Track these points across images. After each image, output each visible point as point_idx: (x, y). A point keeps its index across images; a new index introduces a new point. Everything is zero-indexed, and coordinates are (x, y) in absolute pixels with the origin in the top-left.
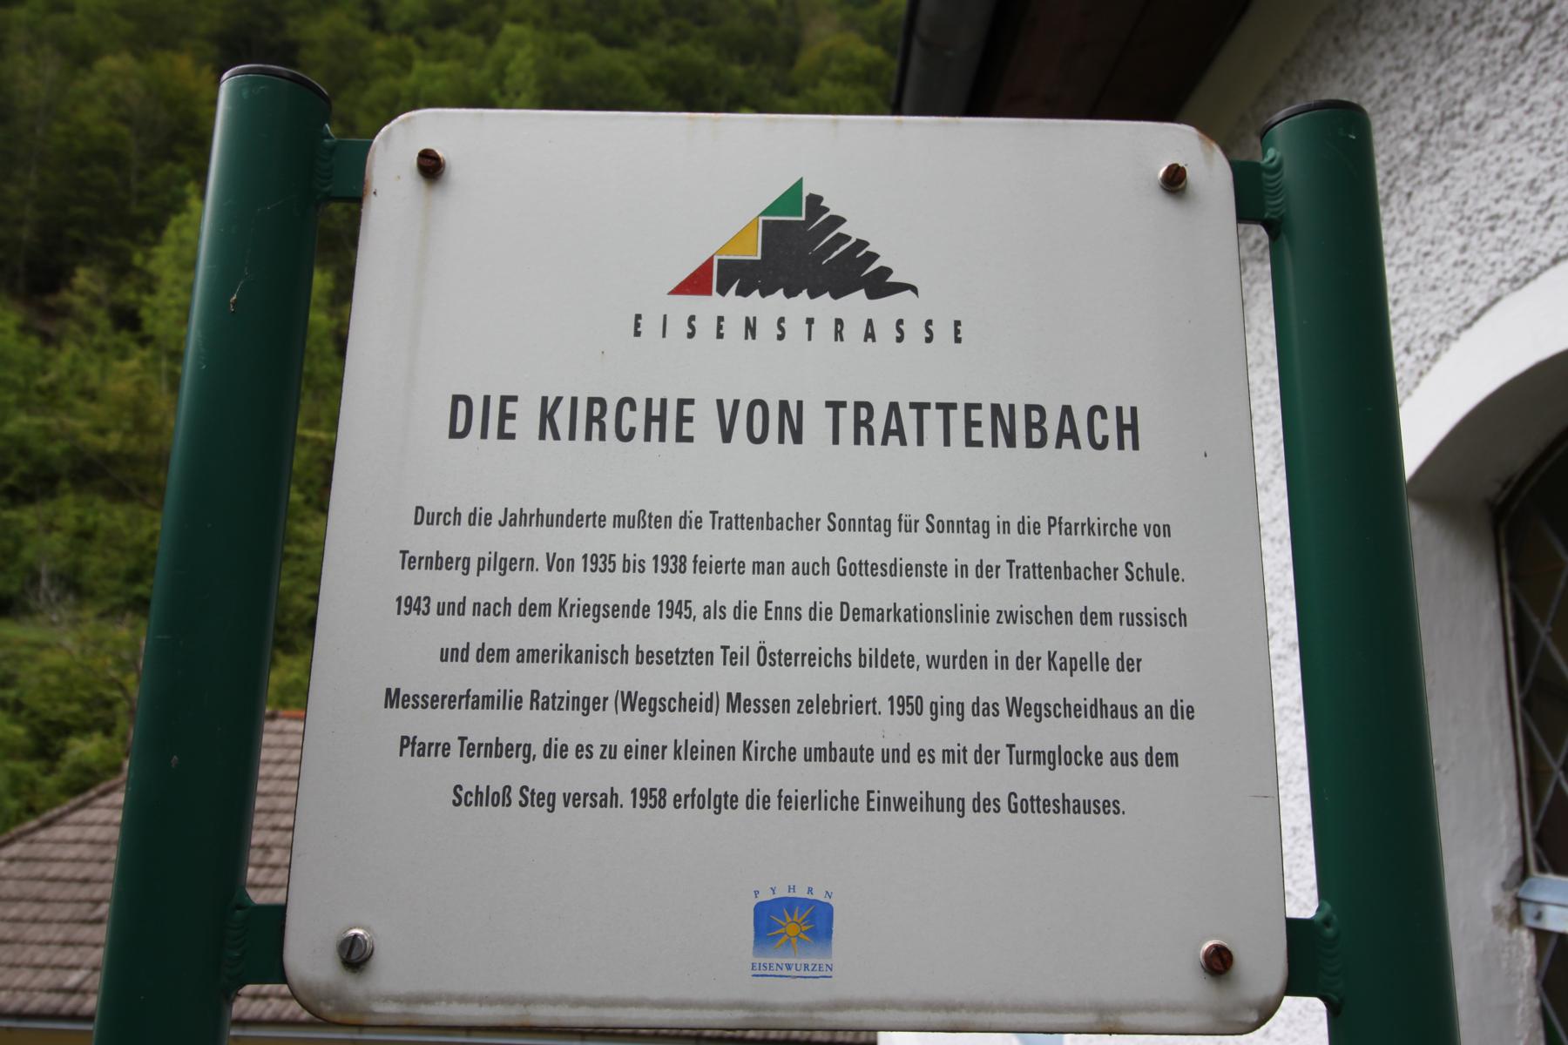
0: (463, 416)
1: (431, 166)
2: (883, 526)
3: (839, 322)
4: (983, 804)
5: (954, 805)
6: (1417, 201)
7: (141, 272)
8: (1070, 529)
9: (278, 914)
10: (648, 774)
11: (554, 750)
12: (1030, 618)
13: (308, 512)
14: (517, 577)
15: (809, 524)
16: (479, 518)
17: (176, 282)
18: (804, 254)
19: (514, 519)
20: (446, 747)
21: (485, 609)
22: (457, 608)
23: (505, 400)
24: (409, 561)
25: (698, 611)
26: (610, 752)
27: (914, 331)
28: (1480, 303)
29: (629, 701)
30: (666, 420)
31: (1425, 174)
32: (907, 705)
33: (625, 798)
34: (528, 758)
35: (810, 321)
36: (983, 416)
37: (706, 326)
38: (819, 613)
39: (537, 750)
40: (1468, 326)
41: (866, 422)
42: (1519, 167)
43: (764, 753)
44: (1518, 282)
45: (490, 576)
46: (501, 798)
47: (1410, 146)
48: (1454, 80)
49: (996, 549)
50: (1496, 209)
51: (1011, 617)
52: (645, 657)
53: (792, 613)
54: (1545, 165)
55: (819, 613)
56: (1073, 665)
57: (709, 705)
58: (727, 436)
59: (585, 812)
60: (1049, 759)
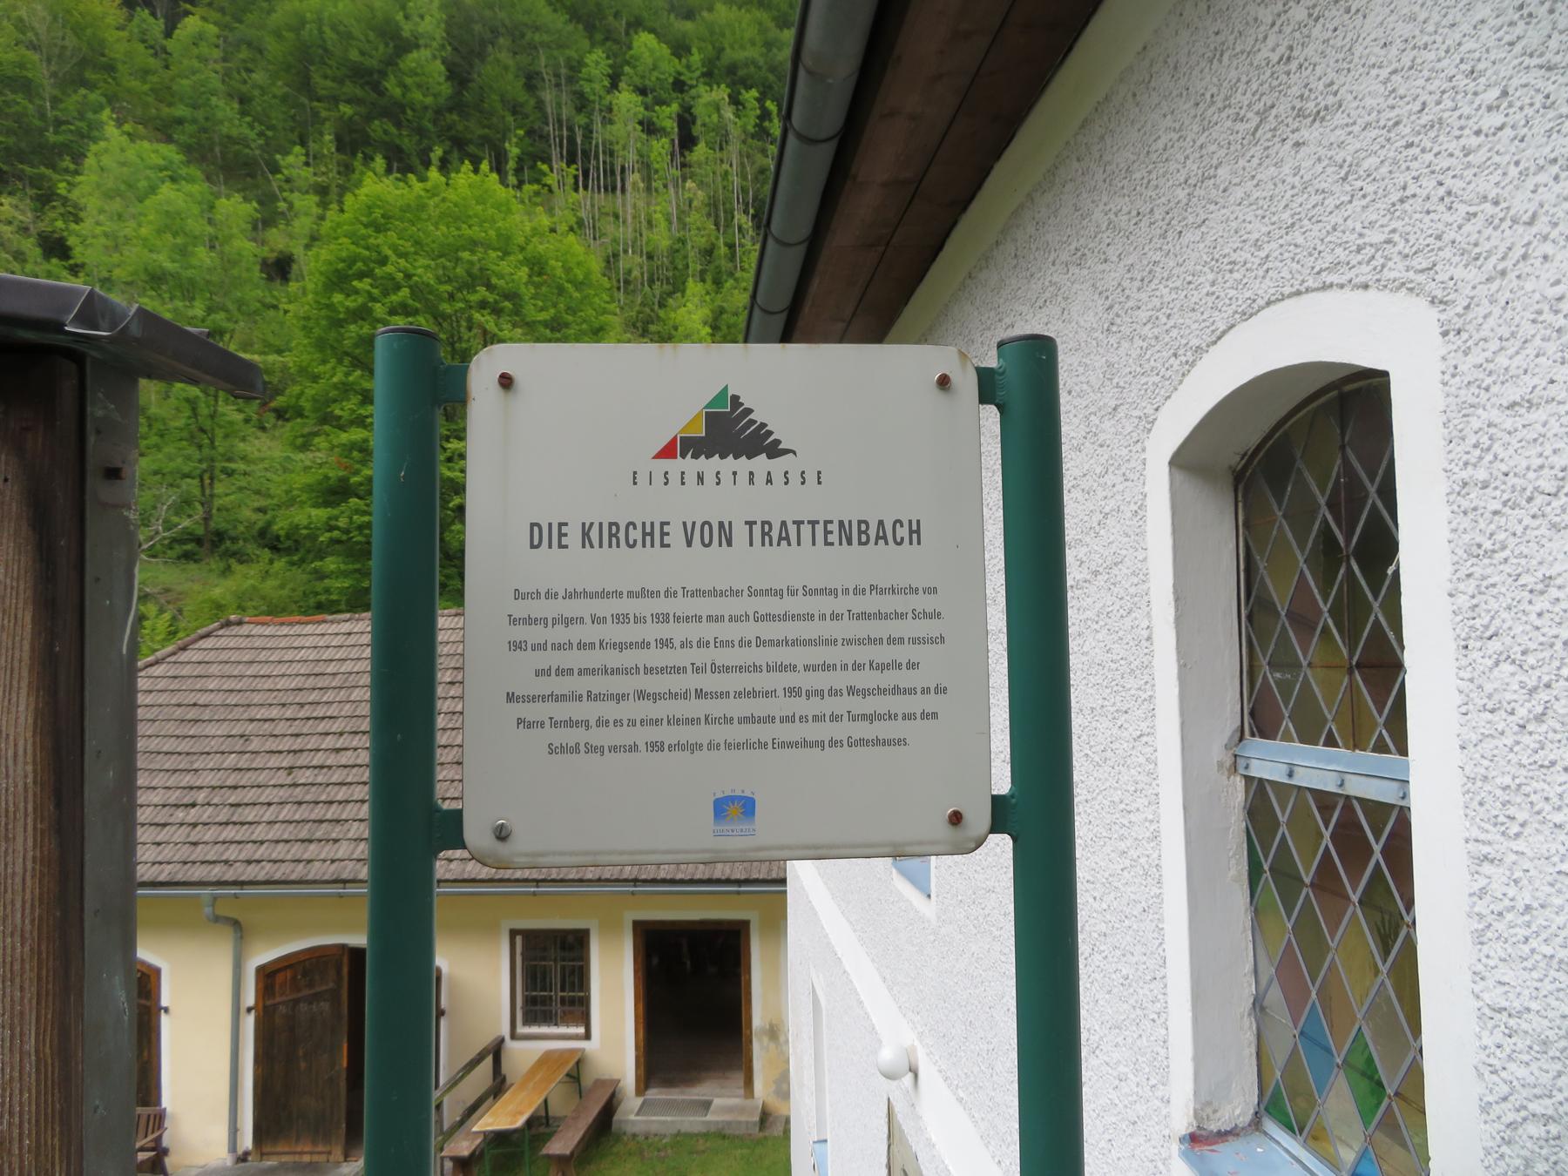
0: (538, 535)
1: (506, 381)
2: (778, 593)
3: (751, 473)
4: (834, 743)
5: (820, 744)
6: (1185, 240)
7: (65, 201)
8: (882, 592)
9: (458, 815)
10: (654, 734)
11: (601, 723)
12: (860, 642)
13: (250, 430)
14: (573, 628)
15: (738, 593)
16: (551, 595)
17: (101, 211)
18: (729, 432)
19: (571, 595)
20: (542, 724)
21: (558, 647)
22: (542, 647)
23: (561, 525)
24: (513, 621)
25: (677, 644)
26: (632, 723)
27: (795, 478)
28: (1223, 327)
29: (642, 695)
30: (654, 535)
31: (1191, 219)
32: (793, 692)
33: (642, 747)
34: (588, 727)
35: (735, 473)
36: (834, 527)
37: (674, 478)
38: (743, 643)
39: (593, 723)
40: (1215, 343)
41: (771, 533)
42: (1249, 227)
43: (716, 720)
44: (1247, 316)
45: (560, 628)
46: (575, 749)
47: (1181, 194)
48: (1213, 148)
49: (841, 604)
50: (1234, 257)
51: (850, 642)
52: (649, 671)
53: (728, 644)
54: (1265, 229)
55: (743, 643)
56: (882, 667)
57: (685, 695)
58: (689, 544)
59: (621, 756)
60: (870, 718)
